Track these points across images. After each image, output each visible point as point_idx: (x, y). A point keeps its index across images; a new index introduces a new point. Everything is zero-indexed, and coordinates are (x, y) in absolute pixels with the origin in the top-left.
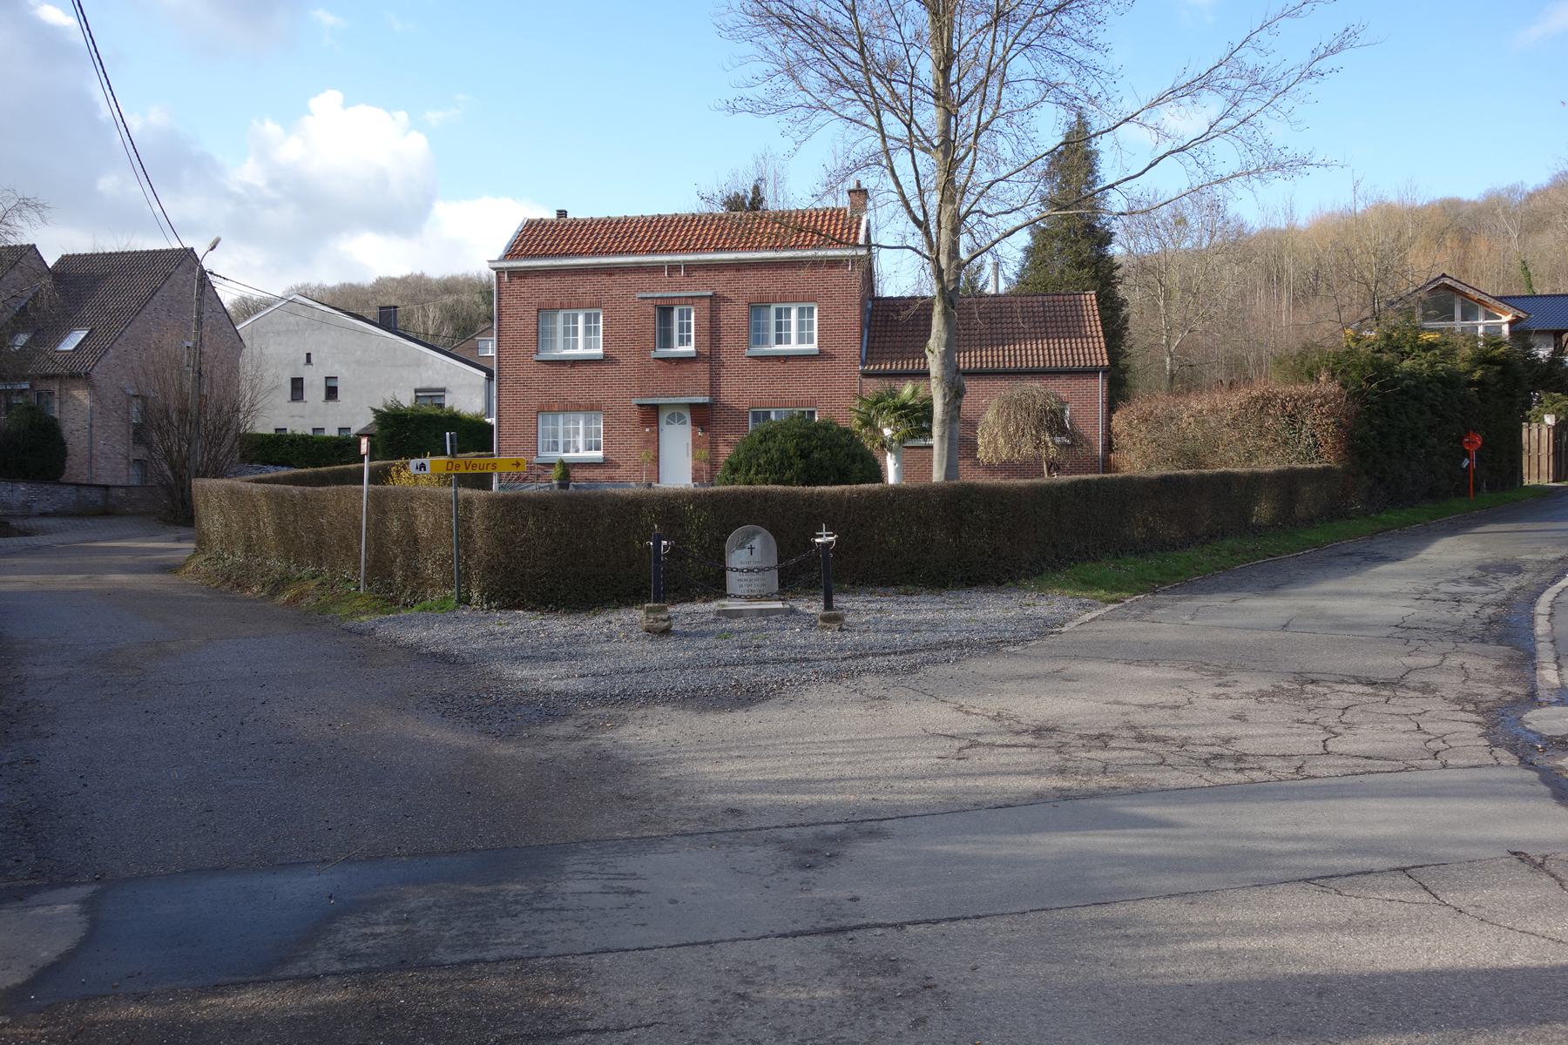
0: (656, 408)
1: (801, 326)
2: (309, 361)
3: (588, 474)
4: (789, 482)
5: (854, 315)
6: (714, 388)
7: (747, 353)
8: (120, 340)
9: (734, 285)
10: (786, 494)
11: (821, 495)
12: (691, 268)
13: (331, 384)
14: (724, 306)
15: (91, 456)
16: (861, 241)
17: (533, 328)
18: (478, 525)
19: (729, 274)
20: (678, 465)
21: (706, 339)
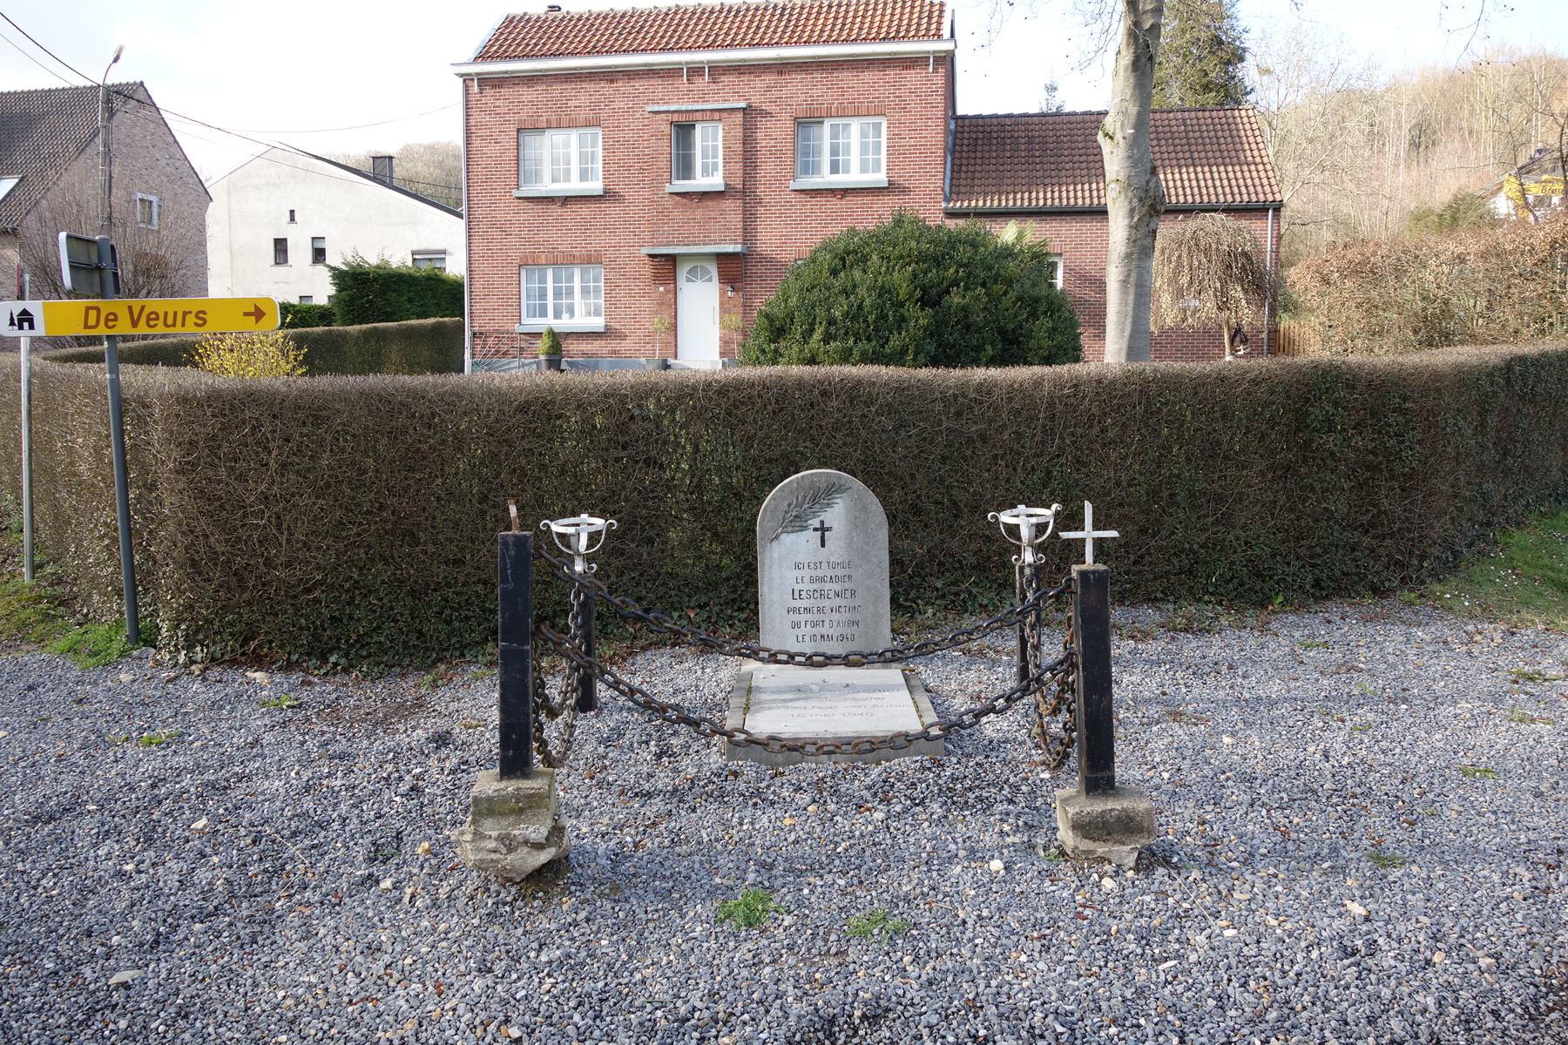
0: (672, 259)
1: (864, 149)
2: (292, 219)
3: (584, 346)
4: (897, 358)
5: (935, 136)
6: (748, 233)
7: (793, 185)
9: (775, 93)
10: (901, 388)
11: (985, 389)
12: (717, 70)
13: (319, 245)
14: (762, 123)
16: (946, 32)
17: (512, 154)
18: (162, 455)
19: (769, 79)
20: (703, 337)
21: (738, 168)
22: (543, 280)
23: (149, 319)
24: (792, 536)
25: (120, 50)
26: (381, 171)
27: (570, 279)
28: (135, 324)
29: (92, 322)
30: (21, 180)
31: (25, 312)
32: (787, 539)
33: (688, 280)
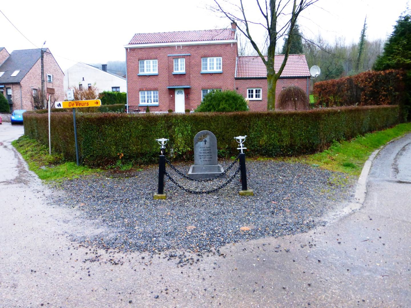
2: (83, 80)
8: (29, 73)
15: (22, 105)
22: (144, 94)
23: (79, 104)
24: (200, 143)
25: (45, 41)
26: (104, 68)
27: (151, 94)
28: (77, 105)
29: (70, 105)
30: (20, 71)
31: (59, 104)
32: (199, 143)
33: (177, 94)
